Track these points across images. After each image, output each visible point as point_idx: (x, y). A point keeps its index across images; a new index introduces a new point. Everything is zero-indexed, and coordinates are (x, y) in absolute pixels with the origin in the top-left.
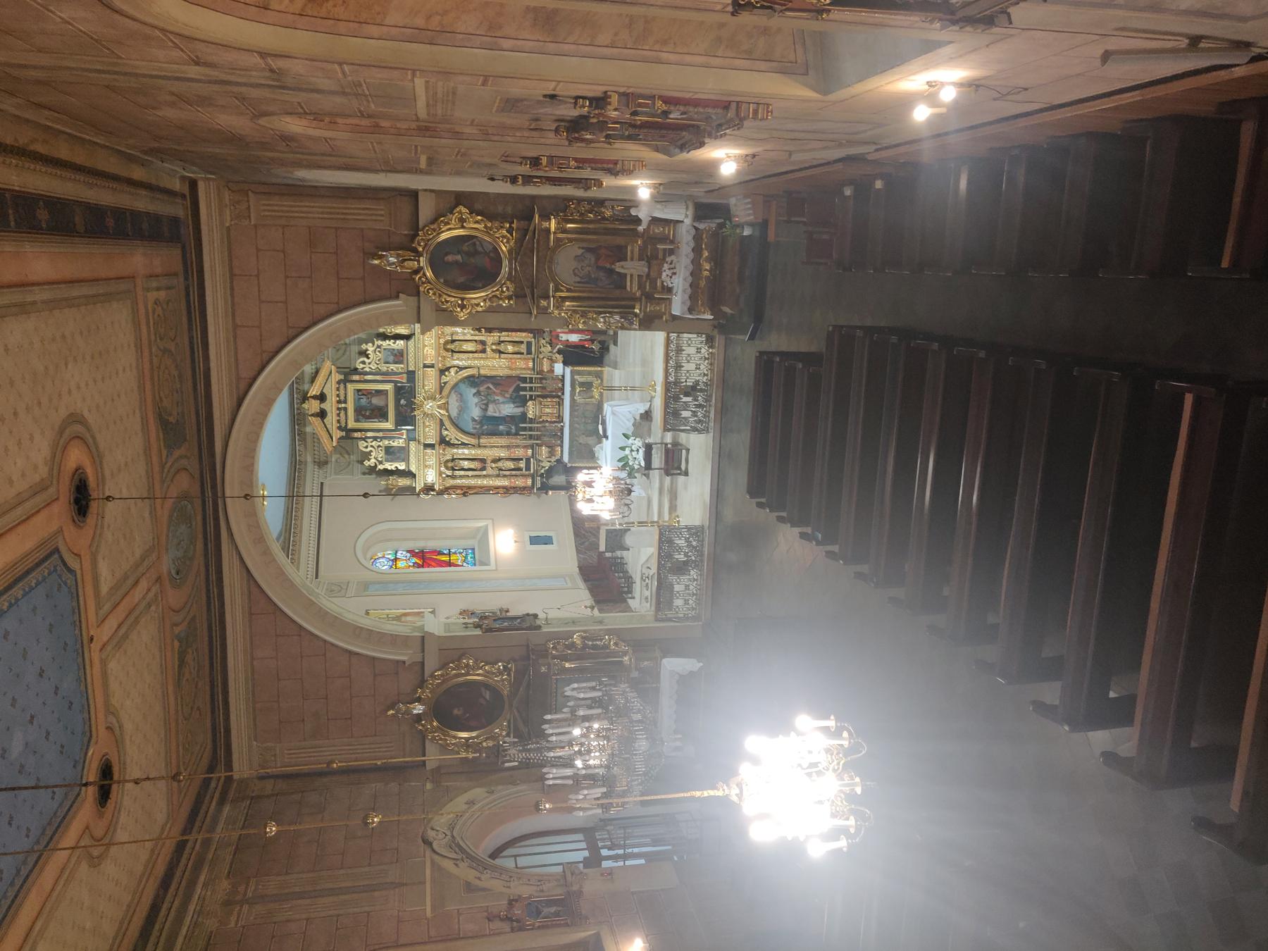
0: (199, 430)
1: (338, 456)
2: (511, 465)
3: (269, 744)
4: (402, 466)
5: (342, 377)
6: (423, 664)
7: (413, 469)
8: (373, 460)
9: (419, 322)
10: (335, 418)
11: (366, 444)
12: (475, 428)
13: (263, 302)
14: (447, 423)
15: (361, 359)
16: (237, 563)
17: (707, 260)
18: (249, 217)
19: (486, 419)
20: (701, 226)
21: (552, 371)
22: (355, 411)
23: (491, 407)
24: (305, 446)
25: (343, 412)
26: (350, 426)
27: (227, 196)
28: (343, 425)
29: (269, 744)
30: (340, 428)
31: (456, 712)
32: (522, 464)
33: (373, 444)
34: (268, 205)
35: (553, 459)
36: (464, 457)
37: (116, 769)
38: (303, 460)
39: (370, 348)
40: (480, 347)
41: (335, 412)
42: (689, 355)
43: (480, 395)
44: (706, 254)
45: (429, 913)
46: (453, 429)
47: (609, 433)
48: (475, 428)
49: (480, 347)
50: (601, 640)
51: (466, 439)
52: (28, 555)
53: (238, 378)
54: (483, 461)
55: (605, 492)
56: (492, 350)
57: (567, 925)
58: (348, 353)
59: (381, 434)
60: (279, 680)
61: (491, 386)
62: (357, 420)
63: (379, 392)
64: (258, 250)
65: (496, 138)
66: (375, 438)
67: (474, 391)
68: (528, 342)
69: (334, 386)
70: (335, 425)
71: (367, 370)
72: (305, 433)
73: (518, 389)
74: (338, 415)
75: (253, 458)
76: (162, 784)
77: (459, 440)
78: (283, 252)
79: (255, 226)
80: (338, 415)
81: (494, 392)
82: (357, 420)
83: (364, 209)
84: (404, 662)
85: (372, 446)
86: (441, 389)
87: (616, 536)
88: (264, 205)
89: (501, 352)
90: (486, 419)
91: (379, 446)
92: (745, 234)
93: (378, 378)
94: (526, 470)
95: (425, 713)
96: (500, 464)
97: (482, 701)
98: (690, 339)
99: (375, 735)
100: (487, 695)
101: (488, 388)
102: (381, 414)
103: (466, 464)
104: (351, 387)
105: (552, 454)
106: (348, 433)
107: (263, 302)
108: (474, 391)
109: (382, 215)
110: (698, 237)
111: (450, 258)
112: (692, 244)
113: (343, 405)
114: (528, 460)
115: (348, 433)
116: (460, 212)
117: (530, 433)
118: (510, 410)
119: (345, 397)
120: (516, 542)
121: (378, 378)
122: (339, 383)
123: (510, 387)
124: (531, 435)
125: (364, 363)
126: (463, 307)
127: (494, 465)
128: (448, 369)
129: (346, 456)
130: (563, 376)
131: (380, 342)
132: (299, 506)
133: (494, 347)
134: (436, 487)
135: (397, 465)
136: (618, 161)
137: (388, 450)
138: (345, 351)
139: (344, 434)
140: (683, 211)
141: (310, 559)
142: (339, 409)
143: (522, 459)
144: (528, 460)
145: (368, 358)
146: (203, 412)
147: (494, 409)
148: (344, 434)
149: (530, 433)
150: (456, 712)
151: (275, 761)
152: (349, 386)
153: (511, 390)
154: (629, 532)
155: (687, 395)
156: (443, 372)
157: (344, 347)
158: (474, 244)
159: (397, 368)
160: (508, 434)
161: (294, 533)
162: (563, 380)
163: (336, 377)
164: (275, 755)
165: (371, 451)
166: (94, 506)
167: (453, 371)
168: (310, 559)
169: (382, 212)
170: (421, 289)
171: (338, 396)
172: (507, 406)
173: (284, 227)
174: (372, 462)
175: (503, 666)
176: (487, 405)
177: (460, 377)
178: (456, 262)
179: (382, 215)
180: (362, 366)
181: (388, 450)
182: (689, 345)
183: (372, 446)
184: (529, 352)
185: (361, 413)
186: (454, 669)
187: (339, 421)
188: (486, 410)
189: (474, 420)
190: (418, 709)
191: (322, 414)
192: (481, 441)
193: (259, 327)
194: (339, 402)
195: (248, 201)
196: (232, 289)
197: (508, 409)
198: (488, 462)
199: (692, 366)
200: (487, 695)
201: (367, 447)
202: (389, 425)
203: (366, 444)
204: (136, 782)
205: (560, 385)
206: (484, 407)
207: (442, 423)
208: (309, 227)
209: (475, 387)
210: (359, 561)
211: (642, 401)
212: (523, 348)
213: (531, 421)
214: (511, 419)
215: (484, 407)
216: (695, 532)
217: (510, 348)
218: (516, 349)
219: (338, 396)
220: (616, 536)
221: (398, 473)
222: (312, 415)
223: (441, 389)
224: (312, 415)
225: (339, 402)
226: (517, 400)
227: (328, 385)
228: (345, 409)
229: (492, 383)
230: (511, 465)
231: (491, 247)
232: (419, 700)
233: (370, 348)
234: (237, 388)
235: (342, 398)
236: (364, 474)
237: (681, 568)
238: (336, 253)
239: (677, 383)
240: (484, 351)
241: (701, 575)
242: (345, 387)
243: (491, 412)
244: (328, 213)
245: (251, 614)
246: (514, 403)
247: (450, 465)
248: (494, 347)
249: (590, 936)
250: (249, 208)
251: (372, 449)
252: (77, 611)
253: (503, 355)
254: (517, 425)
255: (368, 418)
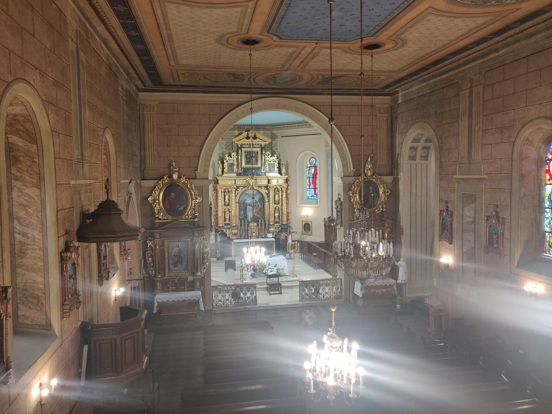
0: (233, 87)
1: (225, 144)
2: (227, 217)
3: (156, 109)
4: (226, 170)
5: (263, 146)
6: (196, 179)
7: (224, 175)
8: (228, 158)
9: (344, 176)
10: (246, 143)
11: (235, 155)
12: (241, 201)
13: (349, 117)
14: (244, 189)
15: (270, 154)
16: (245, 100)
17: (382, 291)
18: (380, 114)
19: (245, 206)
20: (395, 287)
21: (269, 232)
22: (249, 151)
23: (251, 207)
24: (230, 130)
25: (248, 146)
26: (243, 149)
27: (386, 106)
28: (243, 146)
29: (156, 109)
30: (242, 145)
31: (173, 194)
32: (227, 222)
33: (235, 158)
34: (384, 121)
35: (230, 236)
36: (230, 196)
37: (256, 46)
38: (282, 128)
39: (275, 158)
40: (277, 202)
41: (249, 143)
42: (325, 289)
43: (256, 203)
44: (384, 290)
45: (455, 177)
46: (242, 192)
47: (273, 258)
48: (241, 201)
49: (277, 202)
50: (207, 261)
51: (238, 197)
52: (393, 25)
53: (320, 106)
54: (229, 205)
55: (254, 259)
56: (276, 207)
57: (121, 252)
58: (268, 149)
59: (239, 160)
60: (188, 115)
61: (259, 207)
62: (245, 152)
63: (257, 161)
64: (368, 116)
65: (520, 202)
66: (237, 159)
67: (257, 200)
68: (280, 222)
69: (260, 143)
70: (243, 143)
71: (266, 156)
72: (234, 130)
73: (258, 218)
74: (247, 144)
75: (289, 110)
76: (358, 67)
77: (237, 194)
78: (368, 125)
79: (377, 115)
80: (247, 144)
81: (257, 209)
82: (245, 152)
83: (384, 155)
84: (197, 170)
85: (234, 158)
86: (259, 187)
87: (232, 265)
88: (384, 119)
89: (275, 211)
90: (245, 206)
91: (234, 161)
92: (397, 305)
93: (263, 161)
94: (225, 224)
95: (173, 180)
96: (227, 212)
97: (178, 206)
98: (215, 296)
99: (158, 157)
100: (181, 209)
101: (259, 206)
102: (247, 163)
103: (227, 197)
104: (259, 150)
105: (235, 234)
106: (239, 149)
107: (349, 117)
108: (257, 200)
109: (382, 163)
110: (391, 286)
111: (371, 188)
112: (388, 284)
113: (251, 146)
114: (229, 224)
115: (239, 149)
116: (388, 192)
117: (243, 225)
118: (249, 216)
119: (255, 147)
120: (308, 216)
121: (263, 161)
122: (261, 145)
123: (259, 215)
124: (242, 225)
125: (269, 155)
126: (353, 194)
127: (227, 209)
128: (268, 189)
129: (225, 147)
130: (267, 238)
131: (277, 162)
132: (296, 127)
133: (277, 208)
134: (269, 184)
135: (226, 168)
136: (504, 248)
137: (232, 165)
138: (269, 148)
139: (239, 146)
140: (404, 279)
141: (308, 132)
142: (250, 145)
143: (230, 221)
144: (229, 224)
145: (270, 157)
146: (314, 91)
147: (250, 209)
148: (239, 146)
149: (243, 225)
150: (173, 194)
151: (147, 111)
152: (243, 149)
153: (258, 216)
154: (234, 271)
155: (315, 290)
156: (267, 187)
157: (271, 147)
158: (376, 198)
159: (267, 169)
160: (240, 215)
161: (307, 125)
162: (266, 237)
163: (263, 144)
164: (150, 111)
165: (232, 157)
166: (248, 46)
167: (267, 191)
168: (308, 132)
169: (383, 162)
170: (359, 177)
171: (256, 144)
172: (251, 214)
173: (377, 126)
174: (227, 158)
175: (197, 216)
176: (251, 206)
177: (264, 194)
178: (369, 191)
179: (382, 163)
180: (267, 154)
181: (232, 165)
182: (329, 289)
183: (234, 158)
184: (226, 224)
185: (248, 153)
186: (195, 192)
187: (245, 144)
188: (249, 205)
189: (245, 200)
190: (175, 176)
191: (248, 138)
192: (237, 204)
193: (340, 115)
194: (253, 145)
195: (385, 113)
196: (353, 106)
197: (250, 215)
198: (228, 207)
199: (220, 297)
200: (181, 209)
201: (233, 156)
202: (244, 165)
203: (235, 155)
204: (250, 54)
205: (264, 236)
206: (251, 205)
207: (244, 187)
208: (377, 135)
209: (259, 200)
210: (312, 151)
211: (289, 271)
212: (277, 220)
213: (248, 225)
214: (246, 216)
215: (251, 205)
216: (255, 301)
217: (277, 215)
218: (277, 217)
219: (256, 144)
220: (232, 265)
221: (223, 169)
222: (255, 133)
223: (259, 187)
224: (248, 133)
225: (253, 145)
226: (254, 219)
227: (260, 140)
228: (250, 147)
229: (261, 208)
230: (227, 217)
231: (375, 204)
232: (180, 177)
233: (275, 158)
234: (317, 105)
235: (254, 146)
236: (219, 154)
237: (235, 295)
238: (368, 145)
239: (320, 285)
240: (225, 205)
241: (233, 306)
242: (259, 147)
243: (249, 208)
244: (382, 143)
245: (220, 105)
246: (253, 217)
247: (227, 191)
248: (277, 208)
249: (117, 265)
250: (382, 114)
251: (233, 158)
252: (339, 40)
253: (224, 213)
254: (243, 218)
255: (246, 156)
